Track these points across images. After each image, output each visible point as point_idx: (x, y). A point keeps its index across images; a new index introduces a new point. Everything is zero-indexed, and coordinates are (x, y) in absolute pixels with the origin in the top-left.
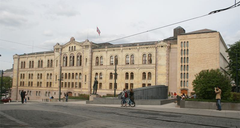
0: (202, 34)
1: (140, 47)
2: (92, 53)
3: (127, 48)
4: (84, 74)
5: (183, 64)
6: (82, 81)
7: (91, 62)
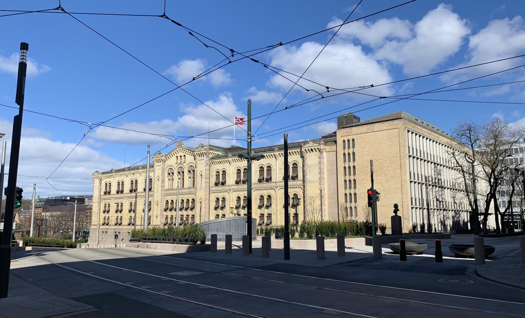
0: (376, 125)
5: (347, 178)
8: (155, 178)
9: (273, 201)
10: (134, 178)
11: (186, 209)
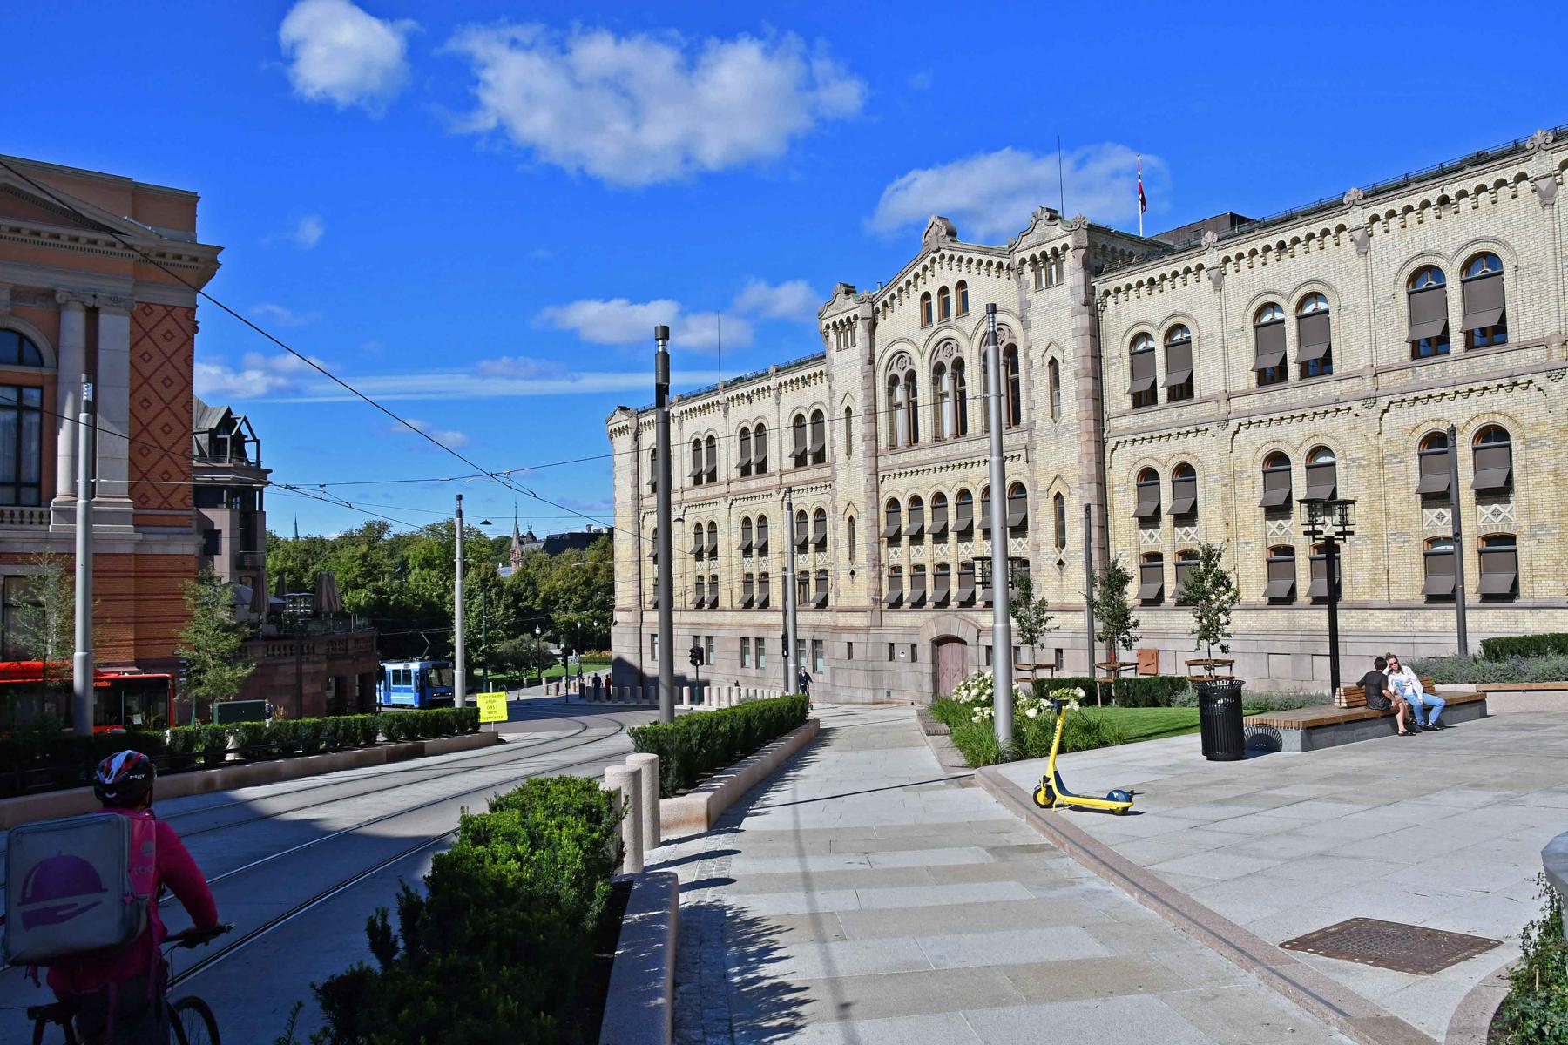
1: (1223, 254)
2: (1093, 307)
3: (1415, 200)
4: (1043, 486)
6: (1037, 546)
7: (1088, 384)
8: (837, 402)
9: (1207, 493)
10: (1281, 277)
11: (917, 538)
